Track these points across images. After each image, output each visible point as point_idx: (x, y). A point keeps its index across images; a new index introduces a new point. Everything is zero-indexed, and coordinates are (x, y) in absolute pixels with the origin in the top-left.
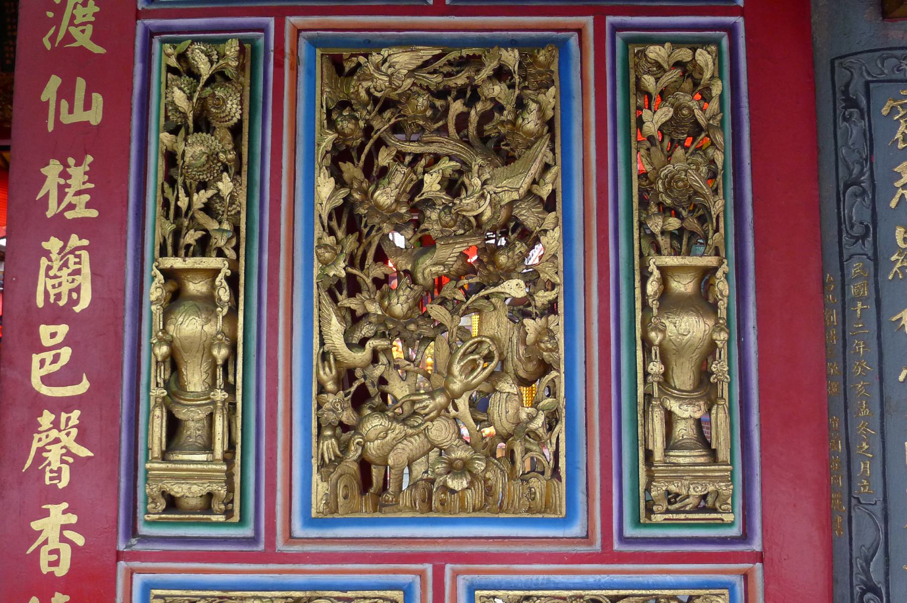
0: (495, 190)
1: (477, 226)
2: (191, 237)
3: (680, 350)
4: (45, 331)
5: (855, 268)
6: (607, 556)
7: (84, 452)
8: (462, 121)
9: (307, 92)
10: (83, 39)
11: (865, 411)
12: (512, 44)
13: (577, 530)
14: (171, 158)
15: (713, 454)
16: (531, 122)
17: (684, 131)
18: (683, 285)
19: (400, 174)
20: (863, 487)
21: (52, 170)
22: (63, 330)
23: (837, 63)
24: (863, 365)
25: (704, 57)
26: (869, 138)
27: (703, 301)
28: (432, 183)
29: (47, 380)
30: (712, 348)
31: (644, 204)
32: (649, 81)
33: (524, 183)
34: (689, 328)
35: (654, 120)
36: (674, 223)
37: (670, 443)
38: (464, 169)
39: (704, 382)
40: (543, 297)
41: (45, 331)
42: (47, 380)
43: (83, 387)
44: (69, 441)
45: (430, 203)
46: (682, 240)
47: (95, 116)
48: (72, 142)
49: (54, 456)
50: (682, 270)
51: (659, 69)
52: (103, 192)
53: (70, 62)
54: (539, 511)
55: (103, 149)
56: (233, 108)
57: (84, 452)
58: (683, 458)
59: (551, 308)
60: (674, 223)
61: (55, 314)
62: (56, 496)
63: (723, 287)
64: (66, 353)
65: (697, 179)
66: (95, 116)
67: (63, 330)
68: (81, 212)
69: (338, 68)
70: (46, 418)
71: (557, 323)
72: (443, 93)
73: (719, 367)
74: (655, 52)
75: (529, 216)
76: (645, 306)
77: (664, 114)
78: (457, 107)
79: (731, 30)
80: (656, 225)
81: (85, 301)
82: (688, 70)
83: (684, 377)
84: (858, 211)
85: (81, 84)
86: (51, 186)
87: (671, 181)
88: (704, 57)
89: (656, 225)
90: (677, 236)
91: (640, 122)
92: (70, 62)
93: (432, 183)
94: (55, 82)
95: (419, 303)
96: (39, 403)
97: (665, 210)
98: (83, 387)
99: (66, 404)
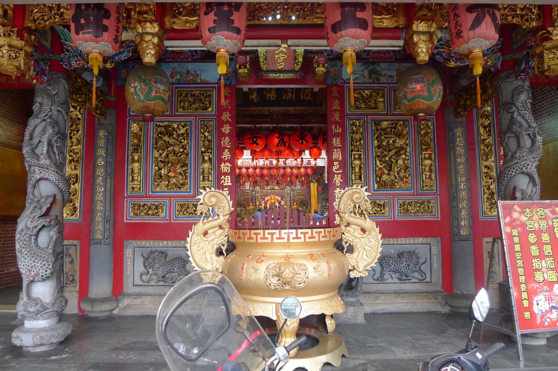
0: (400, 142)
1: (397, 148)
2: (356, 149)
3: (427, 165)
4: (335, 163)
5: (452, 153)
6: (417, 195)
7: (342, 180)
8: (394, 132)
9: (371, 127)
10: (338, 119)
11: (453, 173)
12: (401, 120)
13: (412, 192)
14: (352, 138)
15: (432, 180)
16: (405, 132)
17: (427, 134)
18: (427, 156)
19: (386, 140)
20: (453, 184)
21: (334, 139)
22: (337, 163)
23: (428, 246)
24: (453, 167)
25: (430, 123)
26: (453, 135)
27: (430, 158)
28: (391, 142)
29: (336, 170)
30: (431, 165)
31: (421, 144)
32: (422, 127)
33: (404, 141)
34: (428, 162)
35: (423, 132)
36: (426, 147)
37: (426, 179)
38: (395, 139)
39: (430, 170)
40: (407, 158)
41: (335, 163)
42: (336, 170)
43: (341, 171)
44: (339, 179)
45: (390, 144)
46: (426, 150)
47: (340, 131)
48: (337, 135)
49: (337, 181)
50: (426, 154)
51: (423, 125)
52: (343, 141)
53: (336, 123)
54: (407, 189)
55: (342, 136)
56: (361, 130)
57: (342, 180)
58: (427, 180)
59: (408, 159)
60: (426, 147)
61: (336, 161)
62: (338, 187)
63: (433, 156)
64: (338, 166)
65: (429, 141)
66: (340, 131)
67: (337, 163)
68: (339, 145)
69: (376, 125)
70: (336, 176)
71: (409, 161)
72: (391, 128)
73: (433, 167)
74: (423, 122)
75: (184, 169)
76: (422, 159)
77: (424, 131)
78: (393, 130)
79: (433, 118)
80: (423, 147)
81: (340, 159)
82: (427, 125)
83: (427, 169)
84: (452, 145)
85: (338, 126)
86: (334, 142)
87: (425, 141)
88: (430, 123)
89: (423, 147)
90: (425, 149)
91: (420, 132)
92: (336, 123)
93: (391, 142)
94: (334, 126)
95: (389, 159)
96: (335, 173)
97: (425, 145)
98: (341, 171)
99: (338, 174)
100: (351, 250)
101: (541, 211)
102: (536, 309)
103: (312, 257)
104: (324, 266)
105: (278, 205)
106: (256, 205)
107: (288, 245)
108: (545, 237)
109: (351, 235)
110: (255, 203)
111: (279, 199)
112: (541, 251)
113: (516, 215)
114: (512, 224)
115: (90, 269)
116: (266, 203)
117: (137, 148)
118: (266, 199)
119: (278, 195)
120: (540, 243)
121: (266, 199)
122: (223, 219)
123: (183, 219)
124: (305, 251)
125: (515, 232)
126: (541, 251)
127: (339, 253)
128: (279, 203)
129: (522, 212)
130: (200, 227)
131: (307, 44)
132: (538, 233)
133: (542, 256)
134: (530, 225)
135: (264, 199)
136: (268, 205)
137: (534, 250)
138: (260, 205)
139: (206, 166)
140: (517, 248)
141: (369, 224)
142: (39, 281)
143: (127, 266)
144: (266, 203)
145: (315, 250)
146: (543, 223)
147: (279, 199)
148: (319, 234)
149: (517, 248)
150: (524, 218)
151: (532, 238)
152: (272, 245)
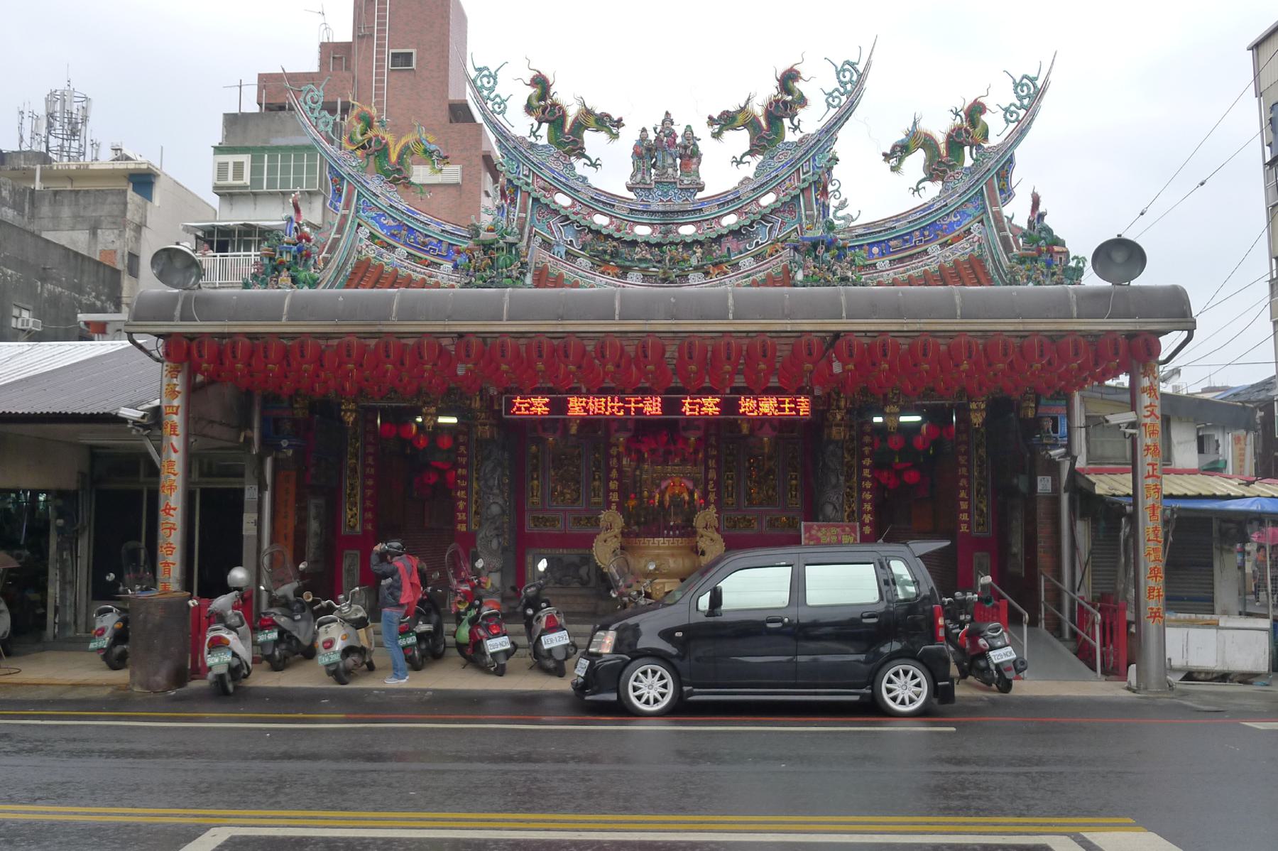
34: (794, 482)
100: (703, 553)
103: (673, 555)
104: (680, 561)
105: (687, 498)
106: (641, 498)
107: (659, 548)
109: (702, 544)
110: (641, 492)
111: (690, 485)
113: (813, 532)
116: (662, 494)
117: (535, 469)
118: (663, 485)
119: (688, 479)
121: (663, 485)
122: (617, 531)
123: (591, 531)
124: (668, 552)
127: (694, 556)
128: (691, 494)
130: (602, 536)
135: (658, 486)
136: (667, 497)
138: (651, 497)
139: (597, 483)
141: (716, 536)
142: (1086, 411)
144: (662, 494)
145: (675, 551)
147: (690, 485)
148: (679, 541)
150: (820, 534)
152: (648, 547)
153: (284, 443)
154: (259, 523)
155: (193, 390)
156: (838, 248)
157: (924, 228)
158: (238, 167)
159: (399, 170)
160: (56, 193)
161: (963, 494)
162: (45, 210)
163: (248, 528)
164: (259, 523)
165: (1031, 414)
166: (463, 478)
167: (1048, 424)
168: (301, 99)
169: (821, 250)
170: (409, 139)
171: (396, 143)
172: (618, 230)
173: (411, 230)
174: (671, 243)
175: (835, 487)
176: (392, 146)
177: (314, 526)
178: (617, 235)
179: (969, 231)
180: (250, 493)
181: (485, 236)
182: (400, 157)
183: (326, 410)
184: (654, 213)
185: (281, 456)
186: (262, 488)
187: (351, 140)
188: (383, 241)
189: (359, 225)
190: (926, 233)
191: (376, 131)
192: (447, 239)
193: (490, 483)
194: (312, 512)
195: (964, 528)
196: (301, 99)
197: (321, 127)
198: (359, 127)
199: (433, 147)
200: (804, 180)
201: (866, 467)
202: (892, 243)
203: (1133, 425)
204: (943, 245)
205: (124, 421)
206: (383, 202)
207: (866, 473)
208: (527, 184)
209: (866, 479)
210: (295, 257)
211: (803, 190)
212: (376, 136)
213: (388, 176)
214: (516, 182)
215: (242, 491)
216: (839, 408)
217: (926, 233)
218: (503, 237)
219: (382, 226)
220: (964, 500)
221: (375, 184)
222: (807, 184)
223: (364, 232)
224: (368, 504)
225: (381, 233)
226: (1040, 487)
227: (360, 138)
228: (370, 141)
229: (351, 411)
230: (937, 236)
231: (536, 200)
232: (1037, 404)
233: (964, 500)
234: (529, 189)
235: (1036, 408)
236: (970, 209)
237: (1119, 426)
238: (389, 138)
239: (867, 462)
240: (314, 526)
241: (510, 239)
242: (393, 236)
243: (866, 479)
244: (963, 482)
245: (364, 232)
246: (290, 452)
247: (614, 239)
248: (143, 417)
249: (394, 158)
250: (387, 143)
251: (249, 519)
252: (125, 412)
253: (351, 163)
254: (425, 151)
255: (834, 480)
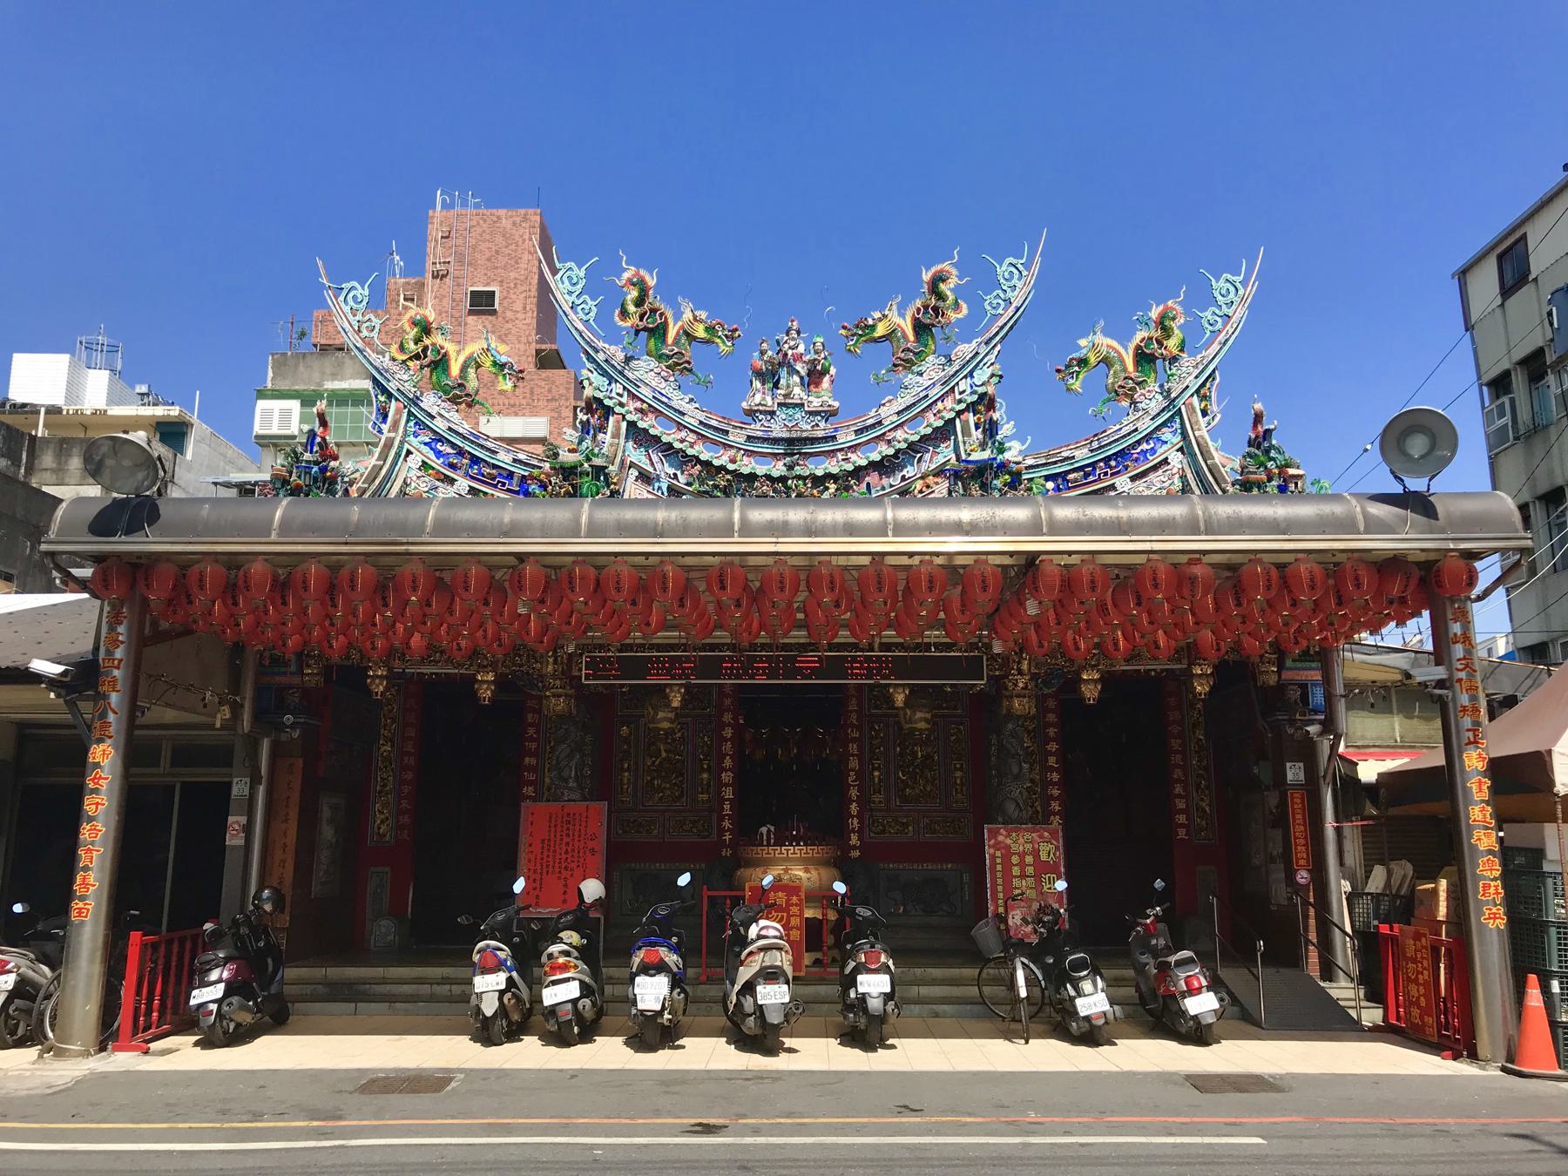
27: (961, 769)
34: (958, 774)
101: (1028, 836)
102: (1010, 922)
104: (814, 874)
108: (1029, 859)
112: (1023, 870)
113: (1001, 838)
114: (997, 846)
115: (106, 943)
120: (1022, 865)
125: (998, 854)
126: (1023, 870)
129: (1009, 836)
131: (408, 1100)
132: (1022, 855)
133: (1023, 876)
134: (1014, 848)
137: (1016, 871)
140: (999, 868)
143: (101, 869)
146: (1029, 846)
149: (999, 868)
150: (1008, 841)
151: (1015, 860)
153: (289, 718)
154: (248, 829)
155: (142, 642)
156: (1010, 473)
157: (1109, 458)
158: (285, 415)
159: (461, 385)
160: (63, 441)
161: (1178, 789)
162: (47, 459)
163: (234, 839)
164: (248, 829)
165: (1272, 680)
166: (532, 769)
167: (1294, 694)
168: (341, 298)
169: (989, 475)
170: (473, 348)
171: (458, 353)
172: (733, 461)
173: (475, 460)
174: (799, 477)
175: (1017, 777)
176: (452, 355)
177: (328, 832)
178: (731, 467)
179: (1165, 461)
180: (239, 788)
181: (567, 457)
182: (464, 369)
183: (350, 676)
184: (776, 441)
185: (284, 737)
186: (255, 780)
187: (402, 348)
188: (439, 472)
189: (409, 453)
190: (1113, 463)
191: (438, 339)
192: (520, 471)
193: (565, 773)
194: (326, 813)
195: (1182, 833)
196: (341, 298)
197: (365, 333)
198: (413, 333)
199: (504, 359)
200: (960, 401)
201: (1052, 754)
202: (1071, 476)
203: (1441, 684)
204: (1133, 479)
205: (37, 678)
206: (440, 425)
207: (1052, 761)
208: (621, 405)
209: (1052, 769)
210: (315, 480)
211: (959, 413)
212: (434, 344)
213: (446, 393)
214: (607, 402)
215: (229, 785)
216: (1020, 672)
217: (1113, 463)
218: (588, 459)
219: (439, 454)
220: (1180, 796)
221: (430, 402)
222: (963, 406)
223: (415, 461)
224: (404, 804)
225: (437, 463)
226: (1290, 776)
227: (412, 346)
228: (425, 349)
229: (381, 677)
230: (1126, 468)
231: (632, 424)
232: (1281, 667)
233: (1180, 796)
234: (623, 411)
235: (1279, 673)
236: (1166, 434)
237: (1424, 685)
238: (450, 347)
239: (1053, 747)
240: (328, 832)
241: (598, 462)
242: (452, 466)
243: (1052, 769)
244: (1178, 774)
245: (415, 461)
246: (296, 734)
247: (728, 472)
248: (64, 674)
249: (455, 369)
250: (446, 354)
251: (236, 821)
252: (41, 666)
253: (403, 379)
254: (495, 363)
255: (1015, 770)
